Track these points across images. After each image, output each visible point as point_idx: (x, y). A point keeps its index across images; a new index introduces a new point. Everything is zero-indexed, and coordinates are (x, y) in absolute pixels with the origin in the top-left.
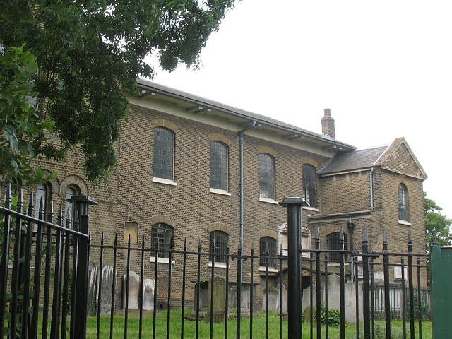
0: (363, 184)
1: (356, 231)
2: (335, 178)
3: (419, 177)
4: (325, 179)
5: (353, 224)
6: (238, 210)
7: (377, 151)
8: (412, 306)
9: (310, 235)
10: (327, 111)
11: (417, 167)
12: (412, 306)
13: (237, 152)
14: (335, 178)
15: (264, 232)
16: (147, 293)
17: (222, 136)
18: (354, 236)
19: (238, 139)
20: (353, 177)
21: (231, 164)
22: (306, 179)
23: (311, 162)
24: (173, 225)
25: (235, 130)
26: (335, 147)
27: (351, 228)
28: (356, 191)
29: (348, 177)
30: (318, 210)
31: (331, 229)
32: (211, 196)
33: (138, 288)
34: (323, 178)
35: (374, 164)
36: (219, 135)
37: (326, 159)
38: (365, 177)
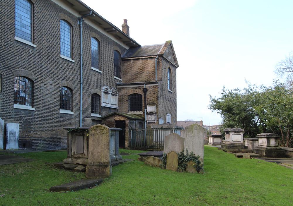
0: (151, 65)
1: (148, 93)
2: (132, 61)
3: (175, 65)
4: (126, 61)
5: (146, 89)
6: (79, 74)
7: (156, 48)
8: (37, 139)
9: (117, 94)
10: (125, 21)
11: (175, 60)
12: (37, 139)
13: (78, 32)
14: (132, 61)
15: (94, 91)
16: (12, 135)
17: (69, 17)
18: (147, 96)
19: (79, 23)
20: (144, 60)
21: (74, 40)
22: (116, 61)
23: (118, 49)
24: (33, 79)
25: (77, 15)
26: (132, 42)
27: (145, 91)
28: (146, 69)
29: (140, 61)
30: (121, 80)
31: (131, 92)
32: (61, 60)
33: (3, 130)
34: (124, 60)
35: (158, 53)
36: (66, 16)
37: (125, 49)
38: (153, 61)
